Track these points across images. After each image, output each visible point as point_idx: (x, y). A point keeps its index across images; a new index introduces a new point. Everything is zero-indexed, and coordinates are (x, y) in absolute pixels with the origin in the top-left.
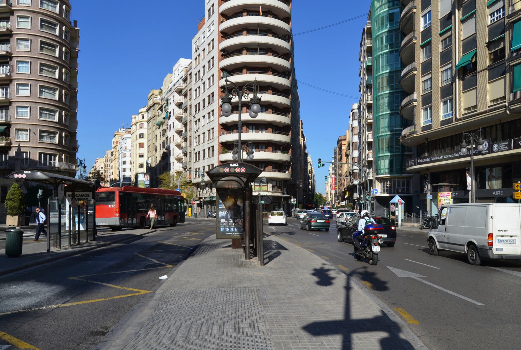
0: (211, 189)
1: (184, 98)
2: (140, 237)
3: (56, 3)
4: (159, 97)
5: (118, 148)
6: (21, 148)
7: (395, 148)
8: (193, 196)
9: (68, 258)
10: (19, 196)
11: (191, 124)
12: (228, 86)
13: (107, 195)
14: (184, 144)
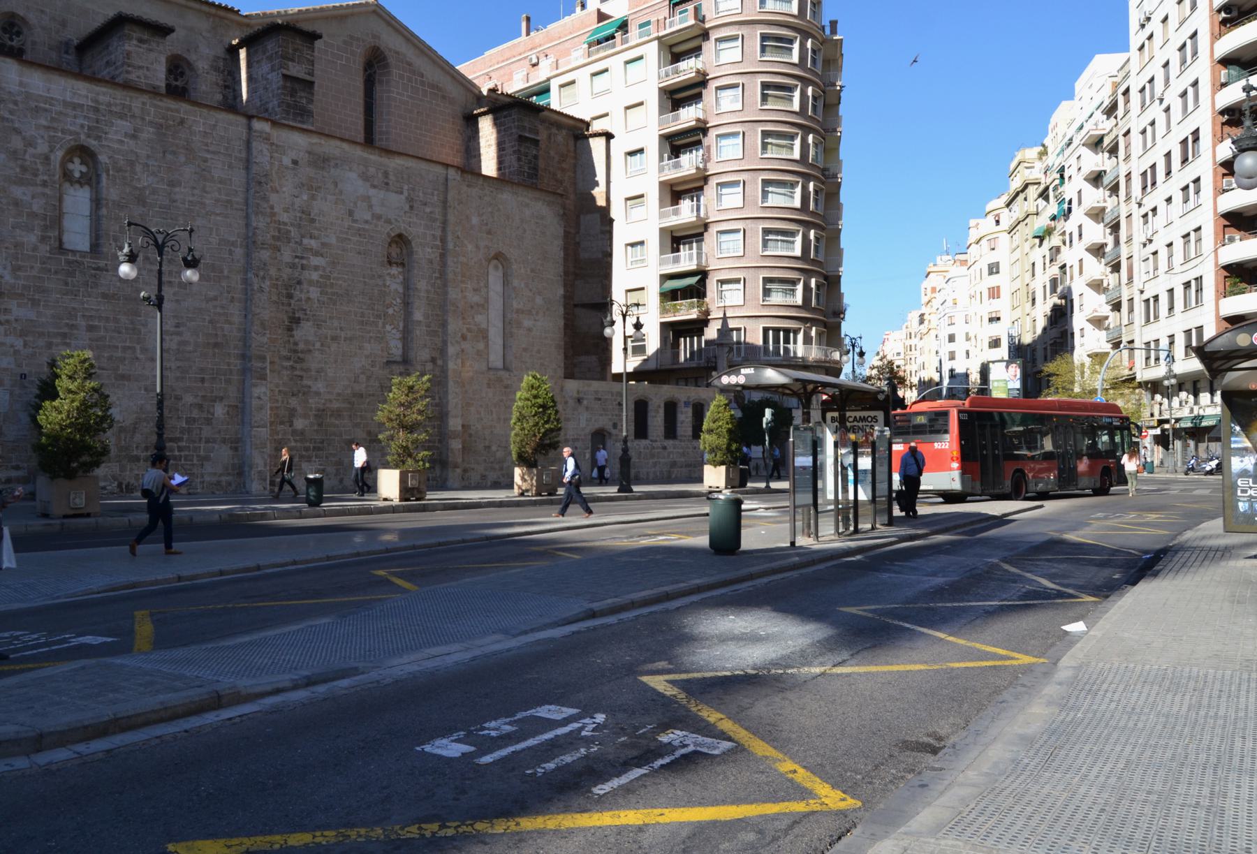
0: (1196, 395)
1: (1110, 158)
2: (1001, 520)
4: (1039, 166)
5: (936, 303)
6: (729, 321)
8: (1140, 417)
9: (835, 562)
10: (727, 423)
11: (1129, 224)
12: (1252, 104)
13: (930, 420)
14: (1111, 280)
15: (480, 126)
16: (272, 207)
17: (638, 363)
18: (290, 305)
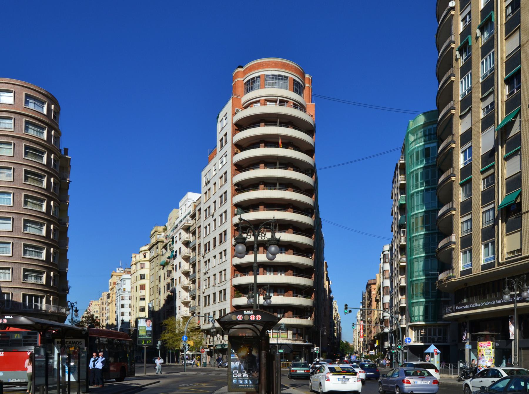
7: (430, 293)
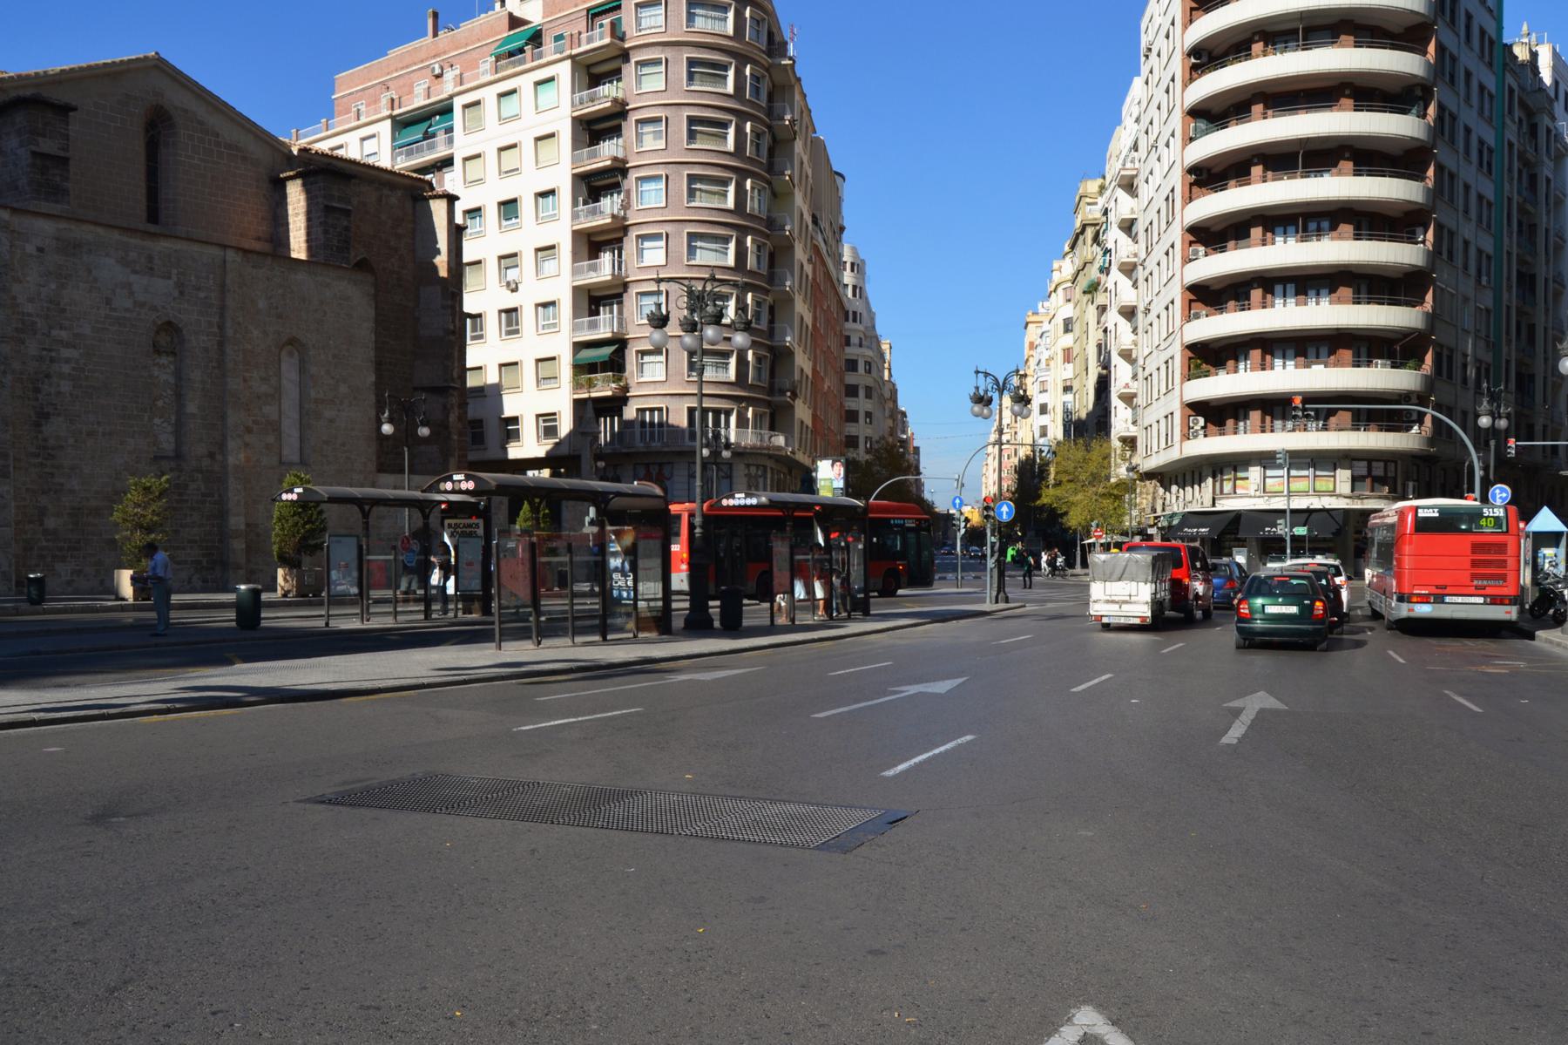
3: (725, 9)
15: (288, 191)
16: (14, 298)
17: (549, 447)
18: (37, 399)
